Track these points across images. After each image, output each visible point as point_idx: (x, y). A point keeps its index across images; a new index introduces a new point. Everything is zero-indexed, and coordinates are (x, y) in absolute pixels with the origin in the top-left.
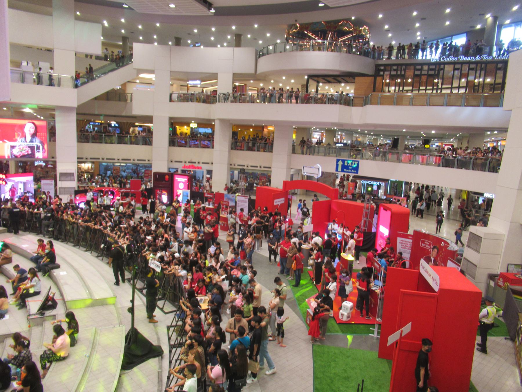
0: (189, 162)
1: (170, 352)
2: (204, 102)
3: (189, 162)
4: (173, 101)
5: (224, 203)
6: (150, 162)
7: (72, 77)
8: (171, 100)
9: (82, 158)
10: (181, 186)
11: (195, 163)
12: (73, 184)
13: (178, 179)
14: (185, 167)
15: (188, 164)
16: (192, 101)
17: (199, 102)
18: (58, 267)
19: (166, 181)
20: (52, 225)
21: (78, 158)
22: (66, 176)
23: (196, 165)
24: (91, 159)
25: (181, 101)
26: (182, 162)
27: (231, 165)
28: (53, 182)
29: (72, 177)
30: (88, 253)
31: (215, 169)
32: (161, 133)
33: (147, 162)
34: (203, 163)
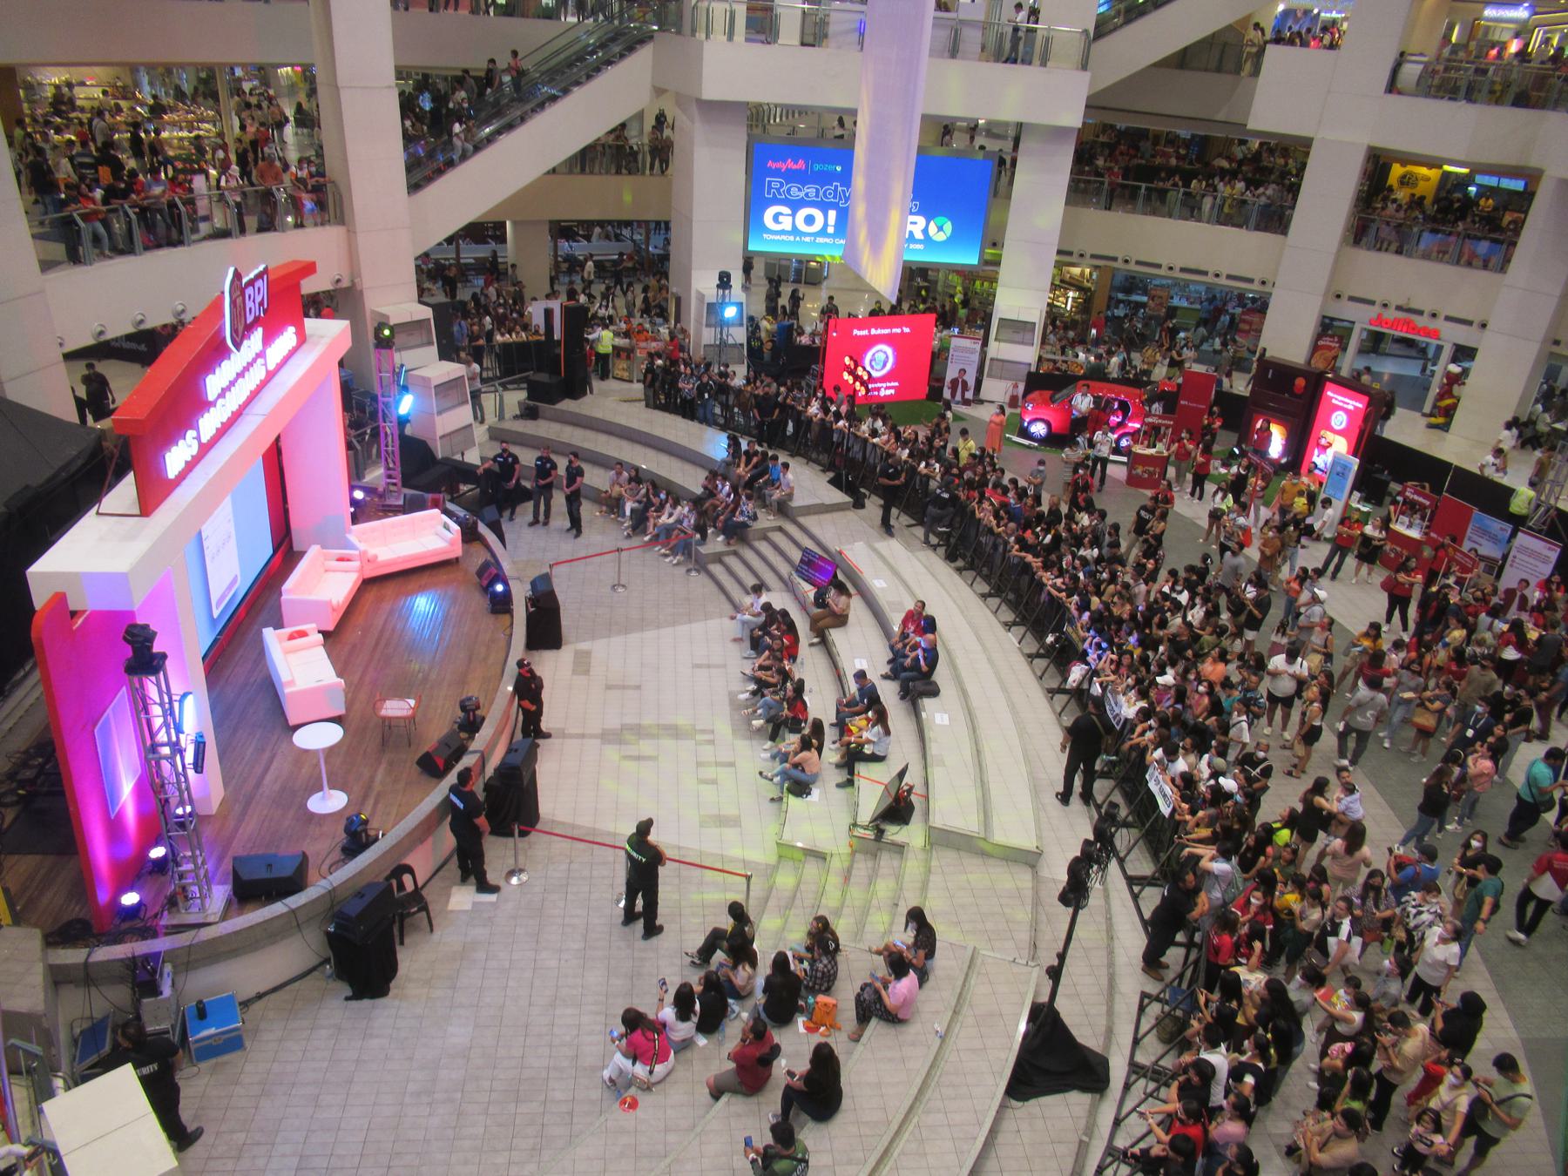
0: (1399, 308)
1: (1127, 1087)
2: (1522, 101)
3: (1399, 308)
4: (1400, 93)
5: (1458, 556)
6: (1266, 289)
7: (1086, 32)
8: (1392, 87)
9: (1070, 254)
10: (1339, 420)
11: (1421, 313)
12: (1027, 354)
13: (1334, 396)
14: (1379, 320)
15: (1391, 314)
16: (1470, 98)
17: (1498, 101)
18: (934, 692)
19: (1293, 394)
20: (947, 521)
21: (1059, 252)
22: (1017, 329)
23: (1421, 322)
24: (1093, 256)
25: (1427, 95)
26: (1372, 303)
27: (1557, 343)
28: (978, 347)
29: (1028, 336)
30: (1011, 638)
31: (1489, 347)
32: (1327, 196)
33: (1256, 286)
34: (1448, 318)
